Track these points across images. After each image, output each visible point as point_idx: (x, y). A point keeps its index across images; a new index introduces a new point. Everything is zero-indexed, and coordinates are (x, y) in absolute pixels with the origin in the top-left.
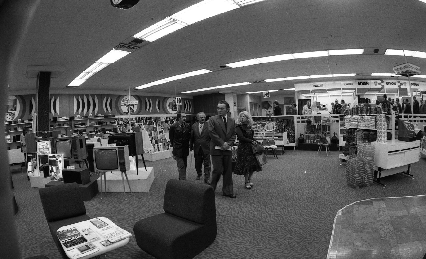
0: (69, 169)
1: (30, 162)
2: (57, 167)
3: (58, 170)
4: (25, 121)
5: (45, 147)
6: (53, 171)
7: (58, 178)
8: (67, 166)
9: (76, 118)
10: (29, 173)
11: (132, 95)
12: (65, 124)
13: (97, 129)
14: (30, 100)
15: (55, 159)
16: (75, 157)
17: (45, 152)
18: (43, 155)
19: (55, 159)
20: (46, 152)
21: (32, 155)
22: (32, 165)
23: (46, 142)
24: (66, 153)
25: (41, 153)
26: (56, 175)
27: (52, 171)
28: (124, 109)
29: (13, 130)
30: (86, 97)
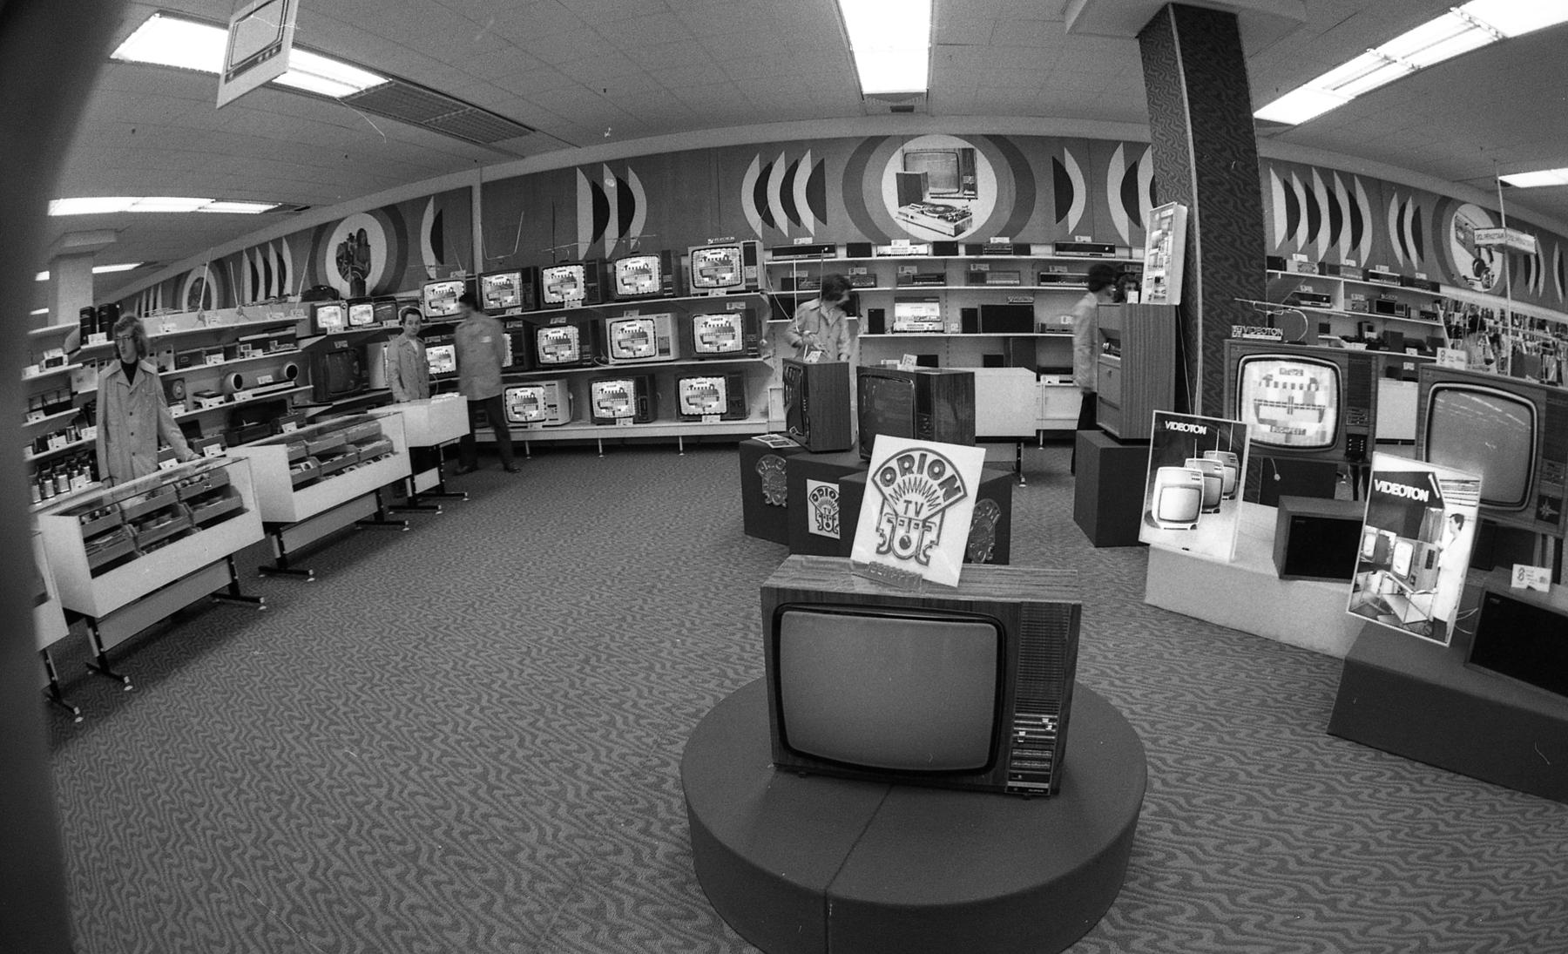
0: (1524, 585)
1: (1182, 465)
2: (1427, 547)
3: (1429, 565)
4: (1034, 249)
5: (1299, 397)
6: (1388, 568)
7: (1414, 616)
8: (1516, 567)
9: (1292, 269)
10: (1157, 526)
11: (1485, 206)
12: (427, 311)
13: (1371, 329)
14: (1054, 160)
15: (1423, 495)
16: (1547, 510)
17: (1293, 425)
18: (1279, 439)
19: (1423, 495)
20: (1302, 426)
21: (1203, 430)
22: (1198, 489)
23: (1309, 371)
24: (1494, 467)
25: (1266, 428)
26: (1401, 593)
27: (1380, 562)
28: (1463, 262)
29: (963, 281)
30: (1324, 182)
